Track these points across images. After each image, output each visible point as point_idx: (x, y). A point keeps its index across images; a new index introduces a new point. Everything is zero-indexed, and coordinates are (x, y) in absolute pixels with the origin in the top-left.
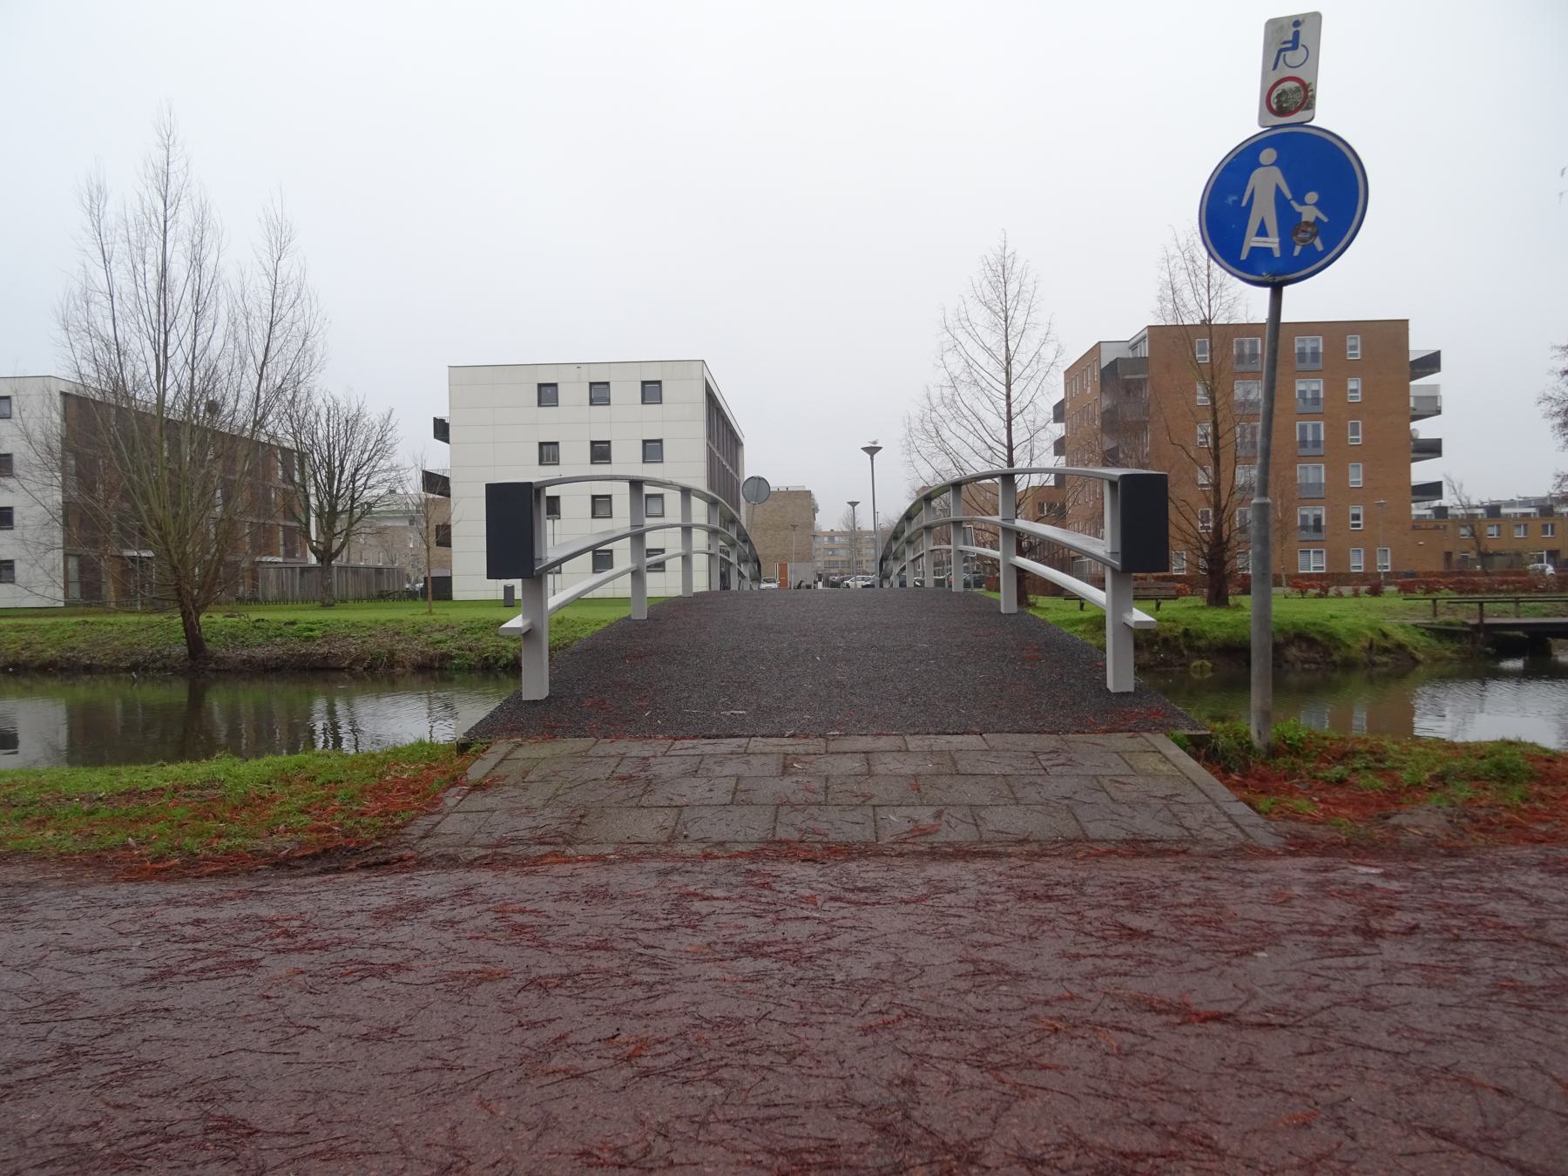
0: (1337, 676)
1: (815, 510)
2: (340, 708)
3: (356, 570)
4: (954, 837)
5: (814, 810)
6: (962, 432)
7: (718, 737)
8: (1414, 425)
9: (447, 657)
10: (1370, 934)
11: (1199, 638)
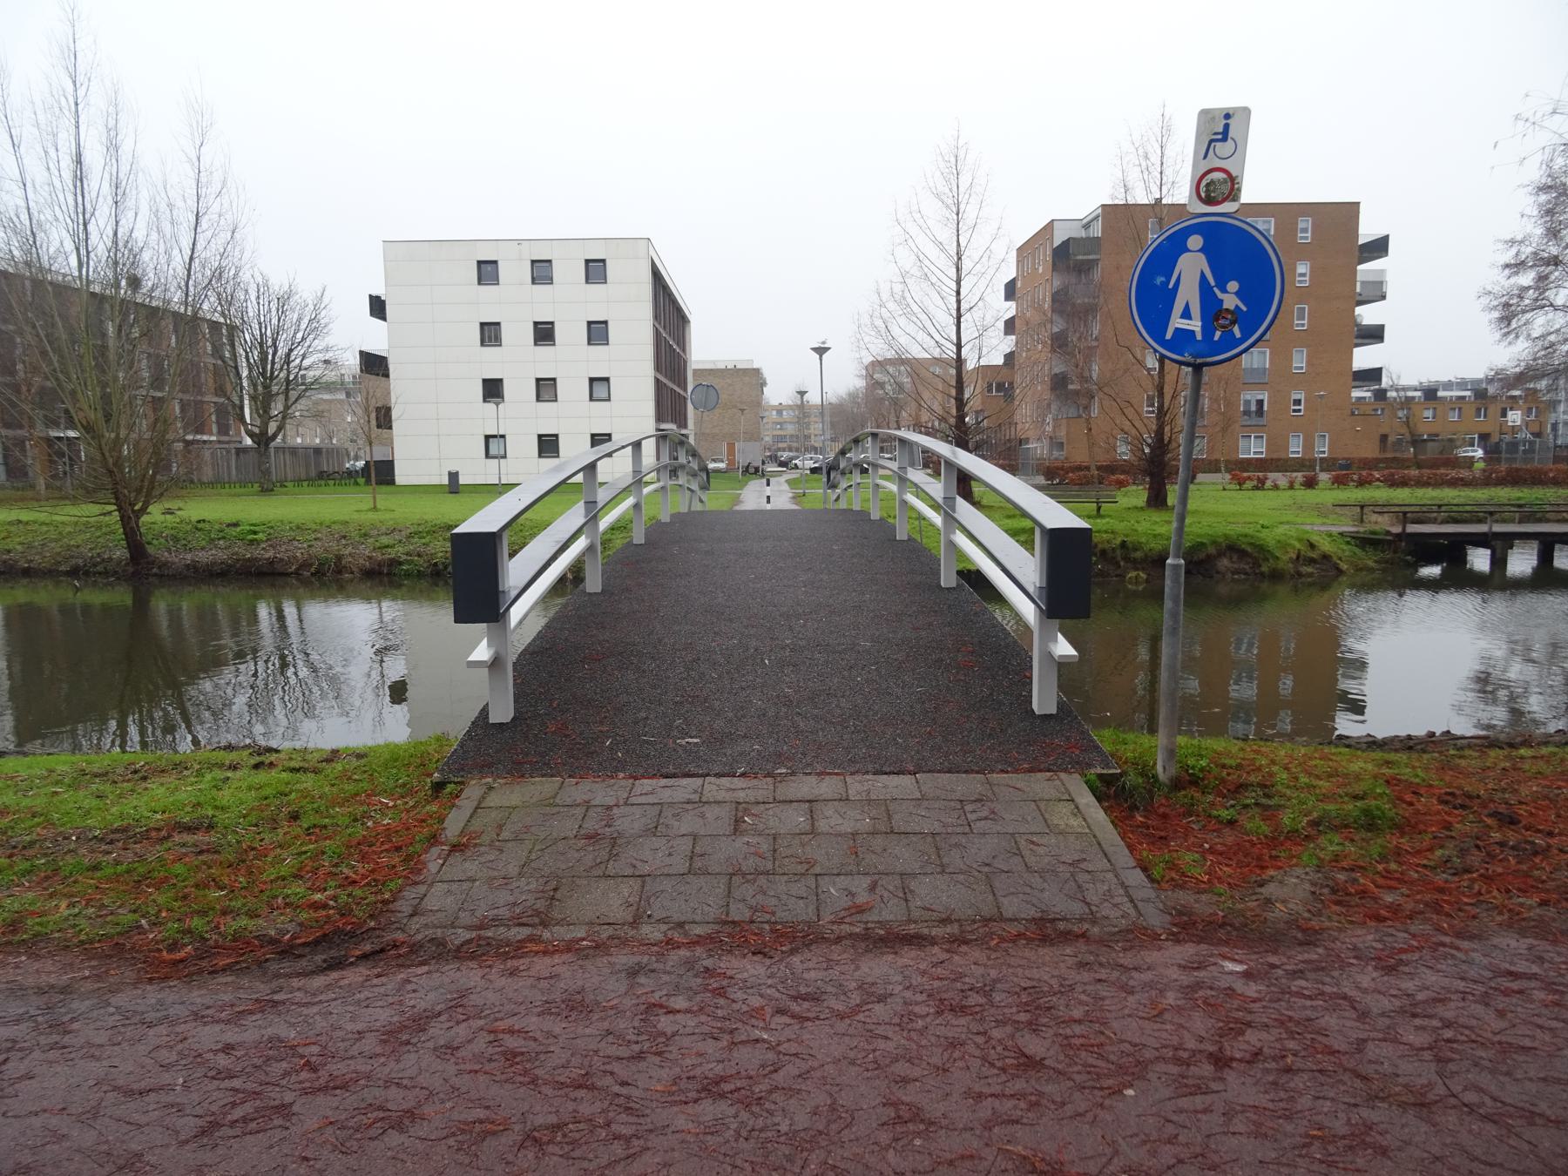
0: (1265, 586)
1: (764, 384)
2: (290, 610)
3: (294, 451)
4: (887, 916)
5: (762, 880)
6: (911, 329)
7: (674, 776)
8: (1359, 310)
9: (395, 562)
10: (1220, 1061)
11: (1135, 550)
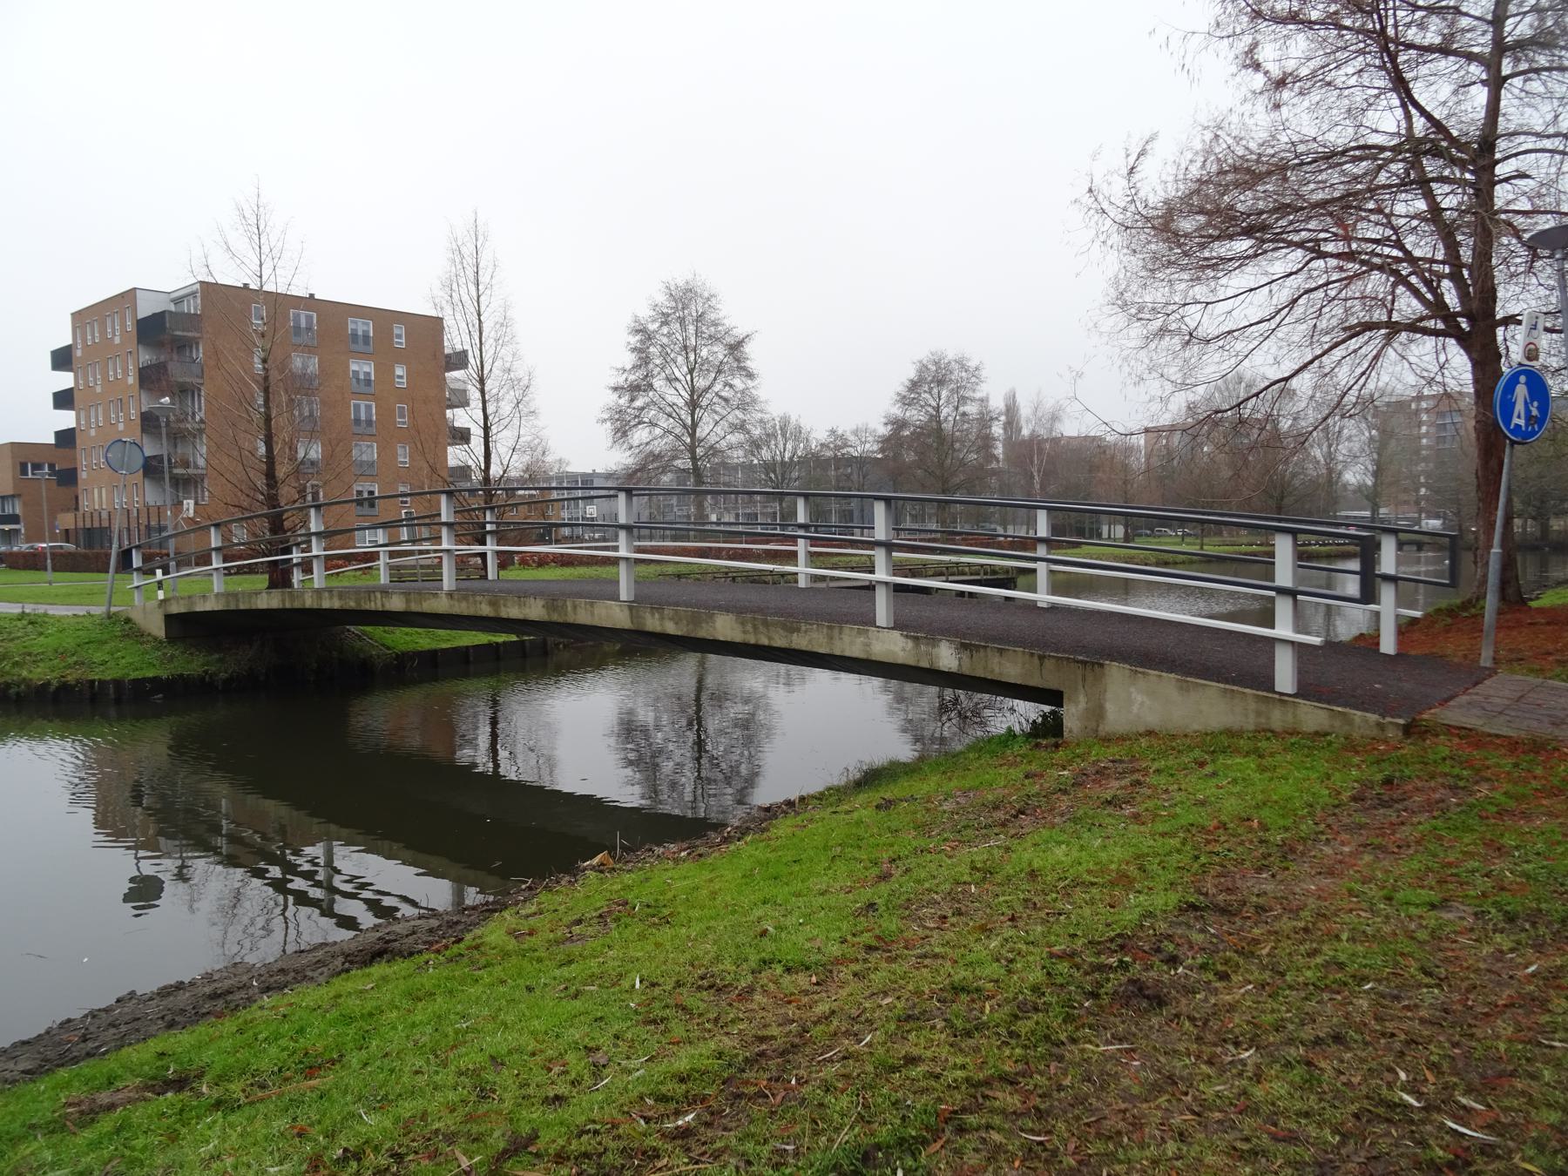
8: (449, 413)
